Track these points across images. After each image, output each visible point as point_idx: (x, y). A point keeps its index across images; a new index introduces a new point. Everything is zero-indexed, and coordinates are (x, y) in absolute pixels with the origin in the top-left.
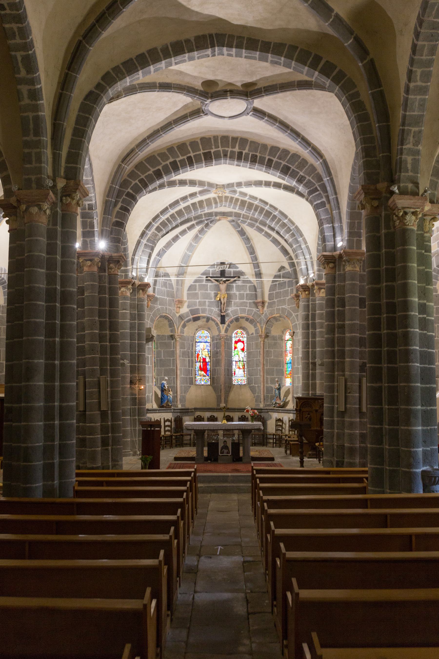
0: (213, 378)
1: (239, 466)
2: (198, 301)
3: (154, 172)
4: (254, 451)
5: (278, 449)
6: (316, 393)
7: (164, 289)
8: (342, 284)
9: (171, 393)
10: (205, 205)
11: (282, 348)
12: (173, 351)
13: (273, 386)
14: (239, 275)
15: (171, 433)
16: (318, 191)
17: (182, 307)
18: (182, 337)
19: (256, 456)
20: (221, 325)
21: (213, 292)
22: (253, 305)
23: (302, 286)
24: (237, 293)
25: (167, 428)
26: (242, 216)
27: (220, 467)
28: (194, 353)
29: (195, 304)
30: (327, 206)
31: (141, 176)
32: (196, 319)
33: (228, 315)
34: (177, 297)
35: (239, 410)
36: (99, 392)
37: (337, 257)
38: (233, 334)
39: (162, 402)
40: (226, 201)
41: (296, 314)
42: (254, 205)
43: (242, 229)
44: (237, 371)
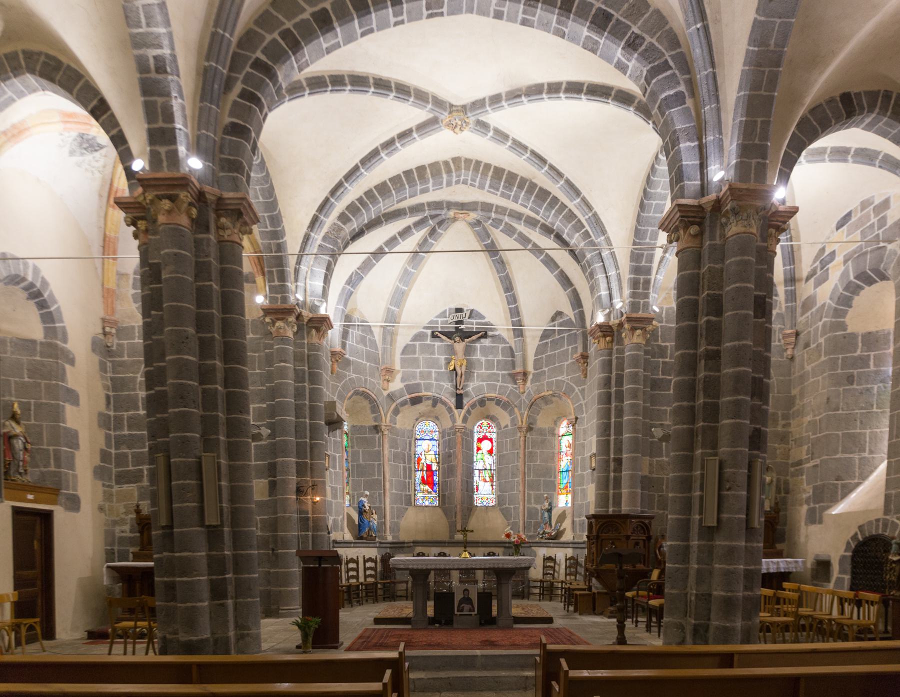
0: (444, 496)
1: (495, 635)
3: (313, 15)
4: (517, 608)
5: (548, 603)
6: (620, 511)
7: (360, 346)
8: (717, 266)
9: (375, 516)
11: (553, 448)
12: (379, 452)
13: (538, 507)
16: (671, 68)
17: (393, 381)
18: (392, 430)
19: (519, 615)
20: (455, 411)
21: (443, 357)
22: (509, 379)
23: (600, 326)
24: (483, 359)
25: (368, 572)
27: (459, 637)
29: (413, 376)
30: (689, 102)
31: (283, 24)
32: (416, 401)
34: (383, 363)
36: (201, 487)
37: (709, 209)
38: (476, 427)
39: (360, 531)
40: (467, 168)
43: (492, 241)
44: (481, 485)
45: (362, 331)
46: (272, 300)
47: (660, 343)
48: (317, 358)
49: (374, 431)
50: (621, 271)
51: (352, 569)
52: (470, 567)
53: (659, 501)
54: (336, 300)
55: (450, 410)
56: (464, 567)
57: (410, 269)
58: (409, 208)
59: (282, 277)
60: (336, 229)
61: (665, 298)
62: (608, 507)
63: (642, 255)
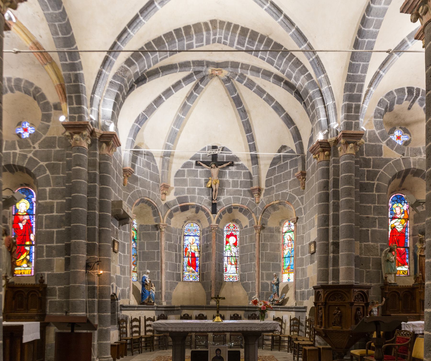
0: (203, 274)
7: (146, 169)
9: (154, 288)
10: (194, 33)
11: (279, 241)
12: (158, 243)
13: (269, 282)
14: (232, 162)
15: (153, 333)
17: (169, 195)
18: (168, 228)
20: (211, 215)
21: (203, 179)
22: (248, 194)
24: (231, 180)
26: (240, 66)
28: (182, 247)
29: (183, 191)
32: (184, 209)
33: (220, 204)
35: (231, 309)
39: (142, 298)
40: (221, 28)
41: (300, 197)
42: (259, 35)
43: (238, 95)
45: (147, 159)
46: (71, 118)
47: (365, 156)
48: (106, 165)
49: (155, 229)
50: (336, 102)
51: (136, 326)
52: (221, 330)
53: (367, 275)
54: (128, 134)
55: (208, 215)
56: (216, 330)
57: (181, 115)
58: (179, 64)
59: (79, 101)
60: (123, 70)
61: (368, 124)
62: (328, 280)
63: (355, 85)
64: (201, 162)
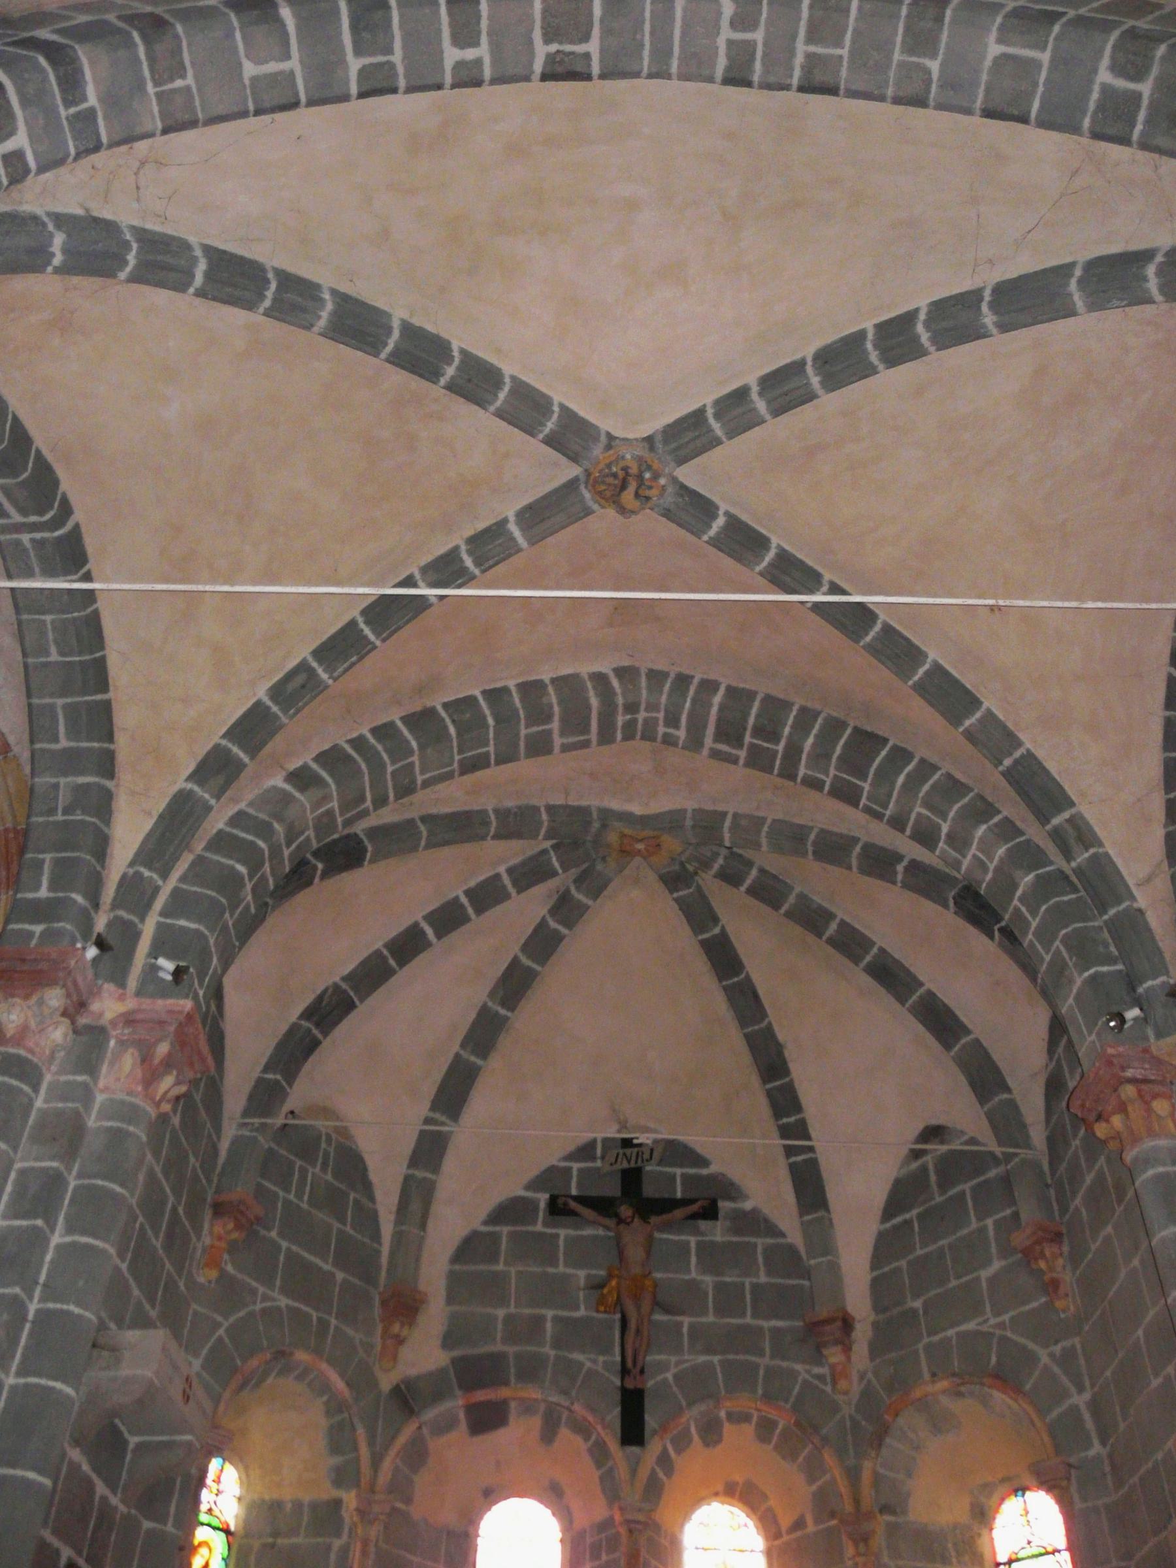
2: (501, 1313)
14: (706, 1202)
24: (708, 1280)
41: (1057, 1349)
64: (575, 1198)
